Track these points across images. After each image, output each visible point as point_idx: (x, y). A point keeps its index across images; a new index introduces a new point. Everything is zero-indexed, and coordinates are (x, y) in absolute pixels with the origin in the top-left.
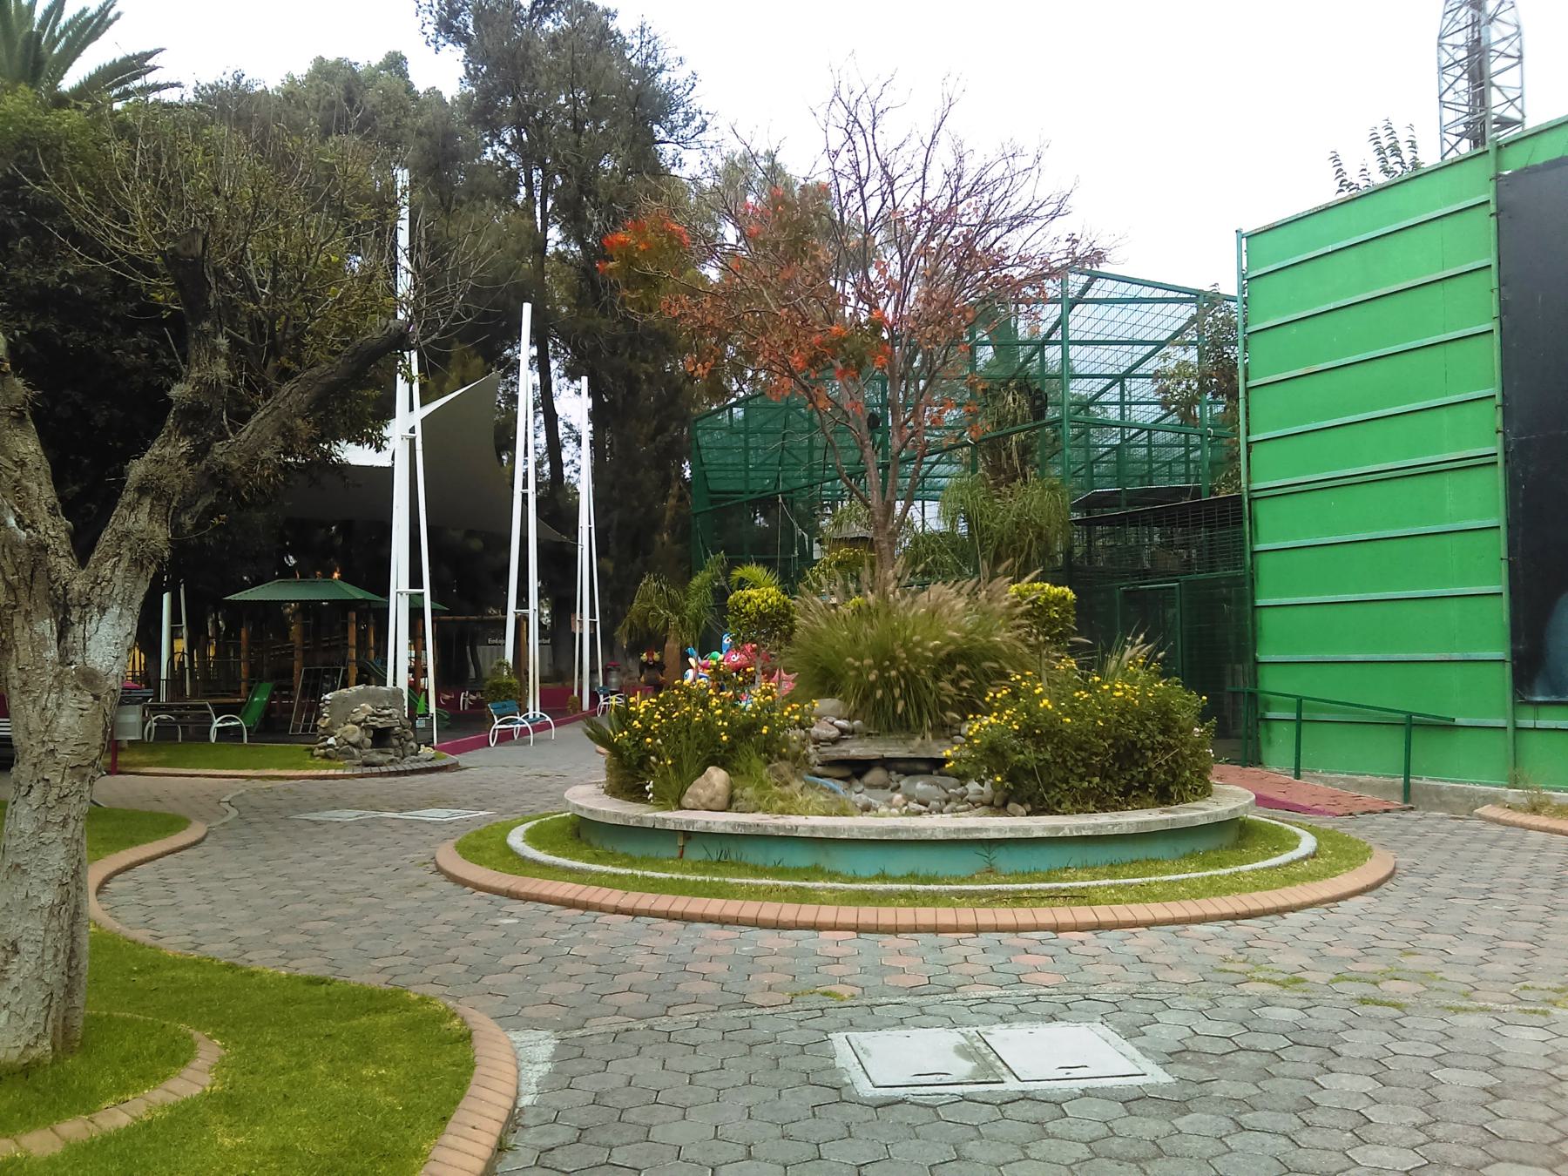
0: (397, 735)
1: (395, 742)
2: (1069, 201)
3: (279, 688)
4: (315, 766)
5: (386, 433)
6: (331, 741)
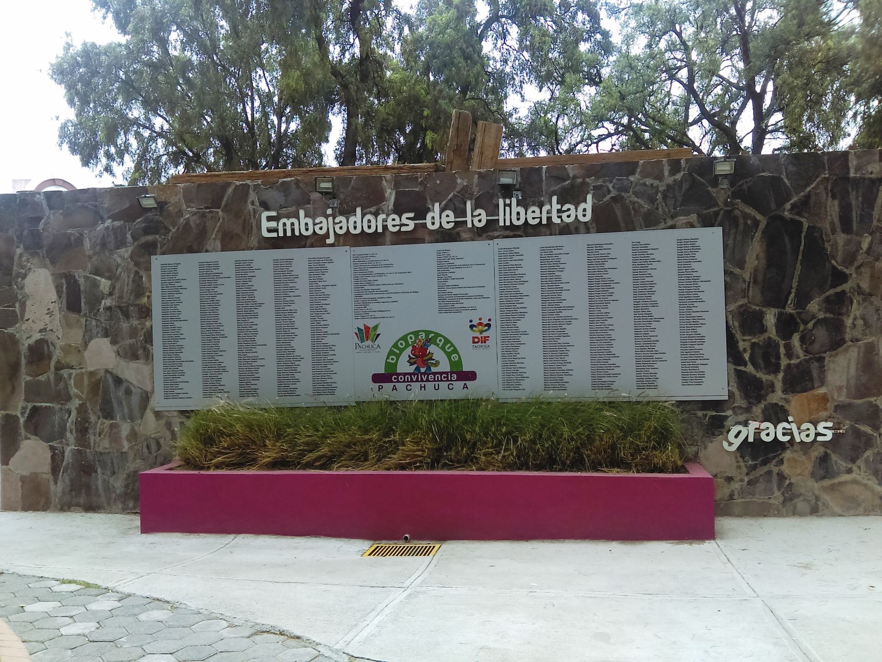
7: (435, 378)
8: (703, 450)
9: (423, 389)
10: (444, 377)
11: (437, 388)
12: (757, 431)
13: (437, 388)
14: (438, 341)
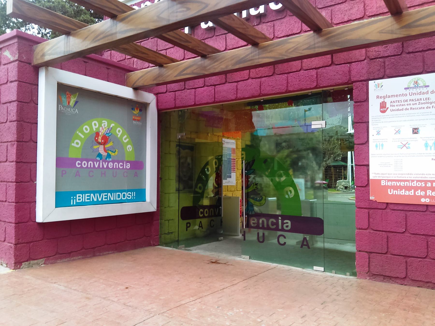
0: (349, 188)
1: (348, 189)
2: (380, 132)
3: (330, 180)
4: (336, 192)
5: (227, 179)
6: (338, 188)
7: (113, 166)
8: (260, 195)
9: (103, 175)
10: (121, 166)
11: (115, 175)
12: (353, 143)
13: (115, 175)
14: (117, 131)
